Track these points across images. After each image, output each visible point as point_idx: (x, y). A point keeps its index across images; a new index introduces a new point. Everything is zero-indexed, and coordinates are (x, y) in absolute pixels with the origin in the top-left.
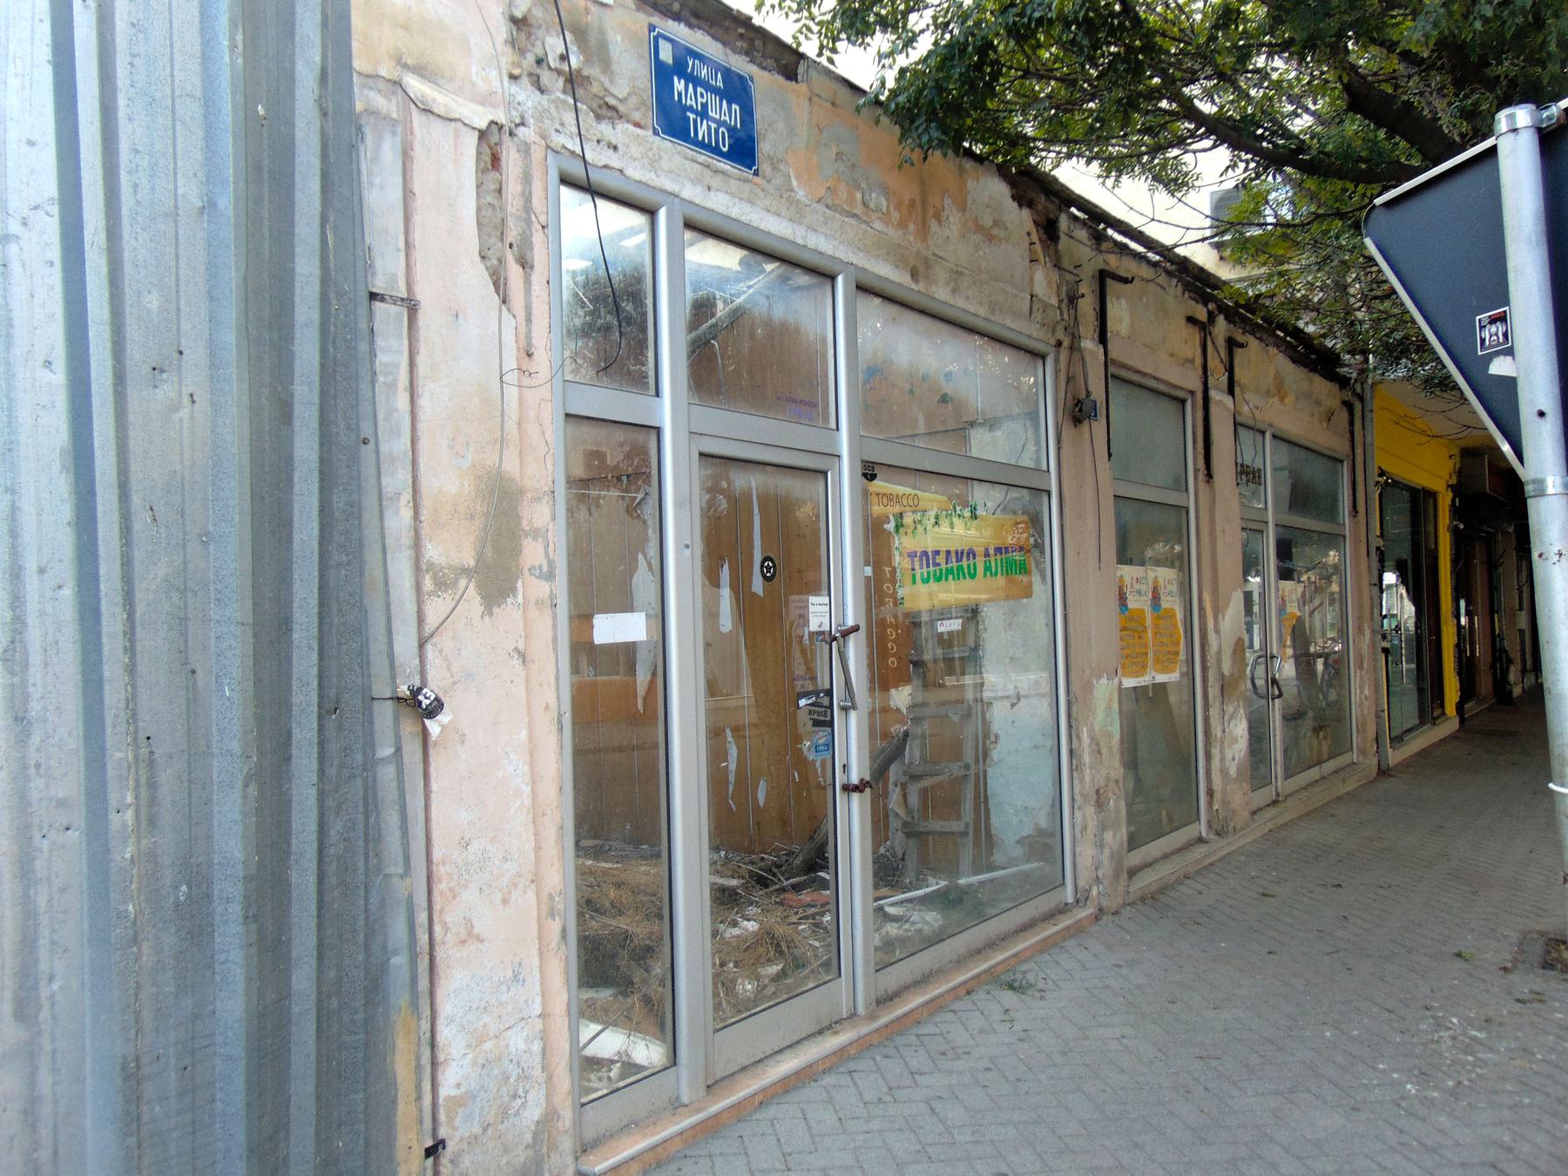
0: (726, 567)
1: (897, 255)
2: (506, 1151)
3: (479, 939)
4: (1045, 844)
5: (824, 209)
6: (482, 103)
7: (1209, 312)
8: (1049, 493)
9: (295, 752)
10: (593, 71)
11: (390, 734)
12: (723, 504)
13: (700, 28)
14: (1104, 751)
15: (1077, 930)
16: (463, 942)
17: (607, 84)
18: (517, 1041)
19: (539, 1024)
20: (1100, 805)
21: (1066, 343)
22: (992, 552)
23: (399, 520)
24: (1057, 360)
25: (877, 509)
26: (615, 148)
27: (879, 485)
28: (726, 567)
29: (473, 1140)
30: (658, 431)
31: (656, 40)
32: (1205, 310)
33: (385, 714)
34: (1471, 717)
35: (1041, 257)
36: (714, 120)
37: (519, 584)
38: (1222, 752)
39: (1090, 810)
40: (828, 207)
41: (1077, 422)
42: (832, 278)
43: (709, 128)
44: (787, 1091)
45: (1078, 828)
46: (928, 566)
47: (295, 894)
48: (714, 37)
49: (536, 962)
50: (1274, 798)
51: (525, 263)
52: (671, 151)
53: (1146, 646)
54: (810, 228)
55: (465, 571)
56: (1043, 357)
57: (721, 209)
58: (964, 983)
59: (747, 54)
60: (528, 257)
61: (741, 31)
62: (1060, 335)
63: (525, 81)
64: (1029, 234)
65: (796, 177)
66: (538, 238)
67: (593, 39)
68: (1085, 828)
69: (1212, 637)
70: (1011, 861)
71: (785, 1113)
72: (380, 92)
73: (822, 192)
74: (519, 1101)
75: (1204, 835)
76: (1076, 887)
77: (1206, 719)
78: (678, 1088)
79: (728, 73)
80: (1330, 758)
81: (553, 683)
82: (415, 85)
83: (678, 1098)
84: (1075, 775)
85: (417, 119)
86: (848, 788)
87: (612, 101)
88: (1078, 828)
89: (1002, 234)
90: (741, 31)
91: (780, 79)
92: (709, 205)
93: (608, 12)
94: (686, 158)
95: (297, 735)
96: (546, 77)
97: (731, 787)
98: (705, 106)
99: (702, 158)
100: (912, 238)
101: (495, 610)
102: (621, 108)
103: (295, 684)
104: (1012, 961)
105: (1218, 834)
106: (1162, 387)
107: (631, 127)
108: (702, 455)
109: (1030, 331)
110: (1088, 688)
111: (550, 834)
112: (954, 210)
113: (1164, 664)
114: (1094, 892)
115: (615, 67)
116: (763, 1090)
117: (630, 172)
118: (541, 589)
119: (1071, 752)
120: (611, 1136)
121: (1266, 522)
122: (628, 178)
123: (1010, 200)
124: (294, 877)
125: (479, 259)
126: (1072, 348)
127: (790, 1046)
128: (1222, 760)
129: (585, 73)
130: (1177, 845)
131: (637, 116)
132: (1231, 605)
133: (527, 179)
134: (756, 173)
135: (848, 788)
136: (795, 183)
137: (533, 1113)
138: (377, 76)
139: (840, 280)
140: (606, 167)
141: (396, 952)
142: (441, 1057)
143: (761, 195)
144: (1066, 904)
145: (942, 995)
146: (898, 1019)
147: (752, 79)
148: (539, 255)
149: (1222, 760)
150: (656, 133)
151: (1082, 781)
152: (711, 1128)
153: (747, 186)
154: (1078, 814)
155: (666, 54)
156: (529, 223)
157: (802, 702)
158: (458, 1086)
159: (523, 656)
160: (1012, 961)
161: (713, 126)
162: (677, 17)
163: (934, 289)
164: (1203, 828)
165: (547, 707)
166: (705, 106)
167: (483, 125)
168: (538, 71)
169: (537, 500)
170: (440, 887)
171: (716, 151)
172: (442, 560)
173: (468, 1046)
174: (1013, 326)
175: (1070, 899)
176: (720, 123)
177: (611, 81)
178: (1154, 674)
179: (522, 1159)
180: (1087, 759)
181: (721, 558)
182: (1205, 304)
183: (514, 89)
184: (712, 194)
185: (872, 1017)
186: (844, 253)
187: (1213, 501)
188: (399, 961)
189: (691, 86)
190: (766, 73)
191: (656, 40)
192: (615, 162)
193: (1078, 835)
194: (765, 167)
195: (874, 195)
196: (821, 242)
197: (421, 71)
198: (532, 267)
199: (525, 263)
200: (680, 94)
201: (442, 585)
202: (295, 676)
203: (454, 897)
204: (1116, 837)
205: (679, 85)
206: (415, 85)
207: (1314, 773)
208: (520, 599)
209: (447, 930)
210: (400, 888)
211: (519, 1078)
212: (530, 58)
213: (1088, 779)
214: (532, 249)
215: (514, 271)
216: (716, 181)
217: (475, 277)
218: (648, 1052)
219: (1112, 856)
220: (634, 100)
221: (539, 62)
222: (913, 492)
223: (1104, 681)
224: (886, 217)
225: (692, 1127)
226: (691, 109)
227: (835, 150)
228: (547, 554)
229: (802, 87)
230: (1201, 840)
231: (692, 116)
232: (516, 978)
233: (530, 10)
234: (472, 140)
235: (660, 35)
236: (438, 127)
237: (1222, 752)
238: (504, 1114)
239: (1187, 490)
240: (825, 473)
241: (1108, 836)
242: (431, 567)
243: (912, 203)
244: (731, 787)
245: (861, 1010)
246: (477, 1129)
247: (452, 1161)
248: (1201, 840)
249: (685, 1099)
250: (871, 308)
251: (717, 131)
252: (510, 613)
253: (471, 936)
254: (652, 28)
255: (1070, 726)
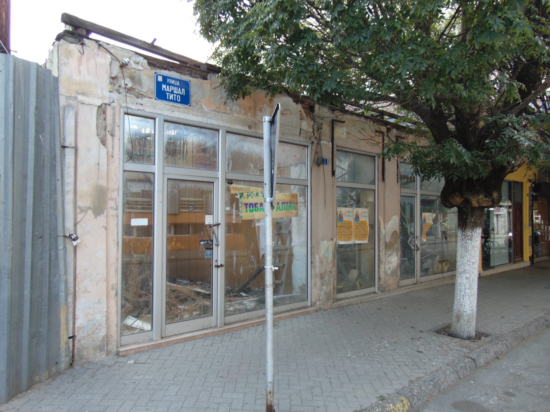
0: (235, 204)
1: (244, 123)
2: (94, 341)
3: (89, 292)
4: (304, 289)
5: (215, 113)
6: (101, 99)
7: (387, 128)
8: (307, 186)
9: (26, 246)
10: (136, 87)
11: (62, 244)
12: (176, 191)
13: (173, 70)
14: (324, 262)
15: (308, 313)
16: (84, 292)
17: (140, 89)
18: (98, 317)
19: (105, 314)
20: (322, 278)
21: (316, 142)
22: (280, 203)
23: (69, 197)
24: (312, 147)
25: (233, 192)
26: (142, 105)
27: (233, 185)
28: (235, 204)
29: (84, 337)
30: (154, 173)
31: (157, 76)
32: (385, 128)
33: (61, 240)
34: (536, 263)
35: (306, 118)
36: (175, 94)
37: (105, 211)
38: (385, 266)
39: (318, 280)
40: (216, 112)
41: (318, 165)
42: (218, 130)
43: (174, 96)
44: (185, 341)
45: (313, 284)
46: (253, 207)
47: (25, 275)
48: (178, 72)
49: (105, 299)
50: (416, 282)
51: (112, 135)
52: (161, 103)
53: (352, 232)
54: (209, 118)
55: (89, 208)
56: (307, 147)
57: (176, 116)
58: (257, 322)
59: (189, 75)
60: (114, 133)
61: (187, 69)
62: (313, 140)
63: (115, 92)
64: (300, 111)
65: (205, 105)
66: (117, 129)
67: (136, 78)
68: (315, 285)
69: (382, 230)
70: (296, 292)
71: (180, 347)
72: (72, 100)
73: (214, 108)
74: (98, 331)
75: (376, 291)
76: (311, 301)
77: (379, 255)
78: (152, 336)
79: (180, 81)
80: (448, 271)
81: (116, 234)
82: (80, 98)
83: (152, 339)
84: (313, 269)
85: (80, 106)
86: (217, 266)
87: (142, 93)
88: (313, 284)
89: (288, 113)
90: (187, 69)
91: (200, 80)
92: (173, 116)
93: (142, 71)
94: (166, 105)
95: (27, 242)
96: (121, 90)
97: (234, 268)
98: (172, 91)
99: (170, 104)
100: (249, 117)
101: (98, 217)
102: (145, 94)
103: (27, 232)
104: (277, 319)
105: (382, 291)
106: (365, 153)
107: (148, 99)
108: (168, 179)
109: (302, 140)
110: (318, 243)
111: (112, 270)
112: (268, 108)
113: (362, 237)
114: (318, 303)
115: (143, 85)
116: (177, 340)
117: (146, 110)
118: (113, 212)
119: (312, 262)
120: (130, 344)
121: (417, 194)
122: (146, 112)
123: (293, 103)
124: (25, 271)
125: (96, 136)
126: (318, 144)
127: (193, 331)
128: (385, 269)
129: (134, 87)
130: (362, 293)
131: (150, 96)
132: (392, 220)
133: (114, 115)
134: (190, 106)
135: (217, 266)
136: (204, 107)
137: (103, 333)
138: (71, 97)
139: (220, 131)
140: (139, 110)
141: (62, 292)
142: (76, 317)
143: (192, 111)
144: (308, 306)
145: (247, 325)
146: (228, 329)
147: (190, 81)
148: (117, 133)
149: (385, 269)
150: (156, 99)
151: (315, 270)
152: (159, 346)
153: (186, 110)
154: (313, 281)
155: (160, 79)
156: (114, 126)
157: (202, 243)
158: (81, 324)
159: (106, 228)
160: (277, 319)
161: (175, 95)
162: (165, 69)
163: (258, 130)
164: (376, 289)
165: (114, 240)
166: (172, 91)
167: (99, 105)
168: (119, 89)
169: (114, 191)
170: (78, 280)
171: (176, 102)
172: (83, 206)
173: (84, 316)
174: (292, 139)
175: (309, 305)
176: (177, 94)
177: (142, 88)
178: (354, 241)
179: (99, 344)
180: (318, 264)
181: (234, 201)
182: (386, 126)
183: (111, 94)
184: (174, 113)
185: (221, 327)
186: (221, 124)
187: (385, 187)
188: (62, 294)
189: (168, 86)
190: (195, 79)
191: (157, 76)
192: (141, 108)
193: (313, 286)
194: (193, 104)
195: (234, 107)
196: (213, 122)
197: (83, 94)
198: (115, 136)
199: (112, 135)
200: (164, 89)
201: (82, 211)
202: (27, 230)
203: (82, 282)
204: (329, 288)
205: (164, 86)
206: (80, 98)
207: (440, 276)
208: (105, 214)
209: (79, 289)
210: (63, 278)
211: (98, 325)
212: (117, 86)
213: (317, 270)
214: (115, 131)
215: (109, 137)
216: (176, 109)
217: (95, 141)
218: (147, 327)
219: (326, 293)
220: (149, 92)
221: (120, 86)
222: (248, 187)
223: (325, 242)
224: (240, 112)
225: (152, 345)
226: (168, 92)
227: (220, 96)
228: (116, 204)
229: (208, 81)
230: (375, 293)
231: (168, 94)
232: (99, 302)
233: (117, 74)
234: (96, 108)
235: (158, 75)
236: (85, 107)
237: (385, 266)
238: (94, 333)
239: (375, 184)
240: (213, 183)
241: (324, 288)
242: (79, 207)
243: (250, 108)
244: (234, 268)
245: (219, 325)
246: (86, 335)
247: (78, 341)
248: (375, 293)
249: (154, 339)
250: (230, 137)
251: (176, 97)
252: (102, 219)
253: (86, 291)
254: (156, 73)
255: (311, 255)
